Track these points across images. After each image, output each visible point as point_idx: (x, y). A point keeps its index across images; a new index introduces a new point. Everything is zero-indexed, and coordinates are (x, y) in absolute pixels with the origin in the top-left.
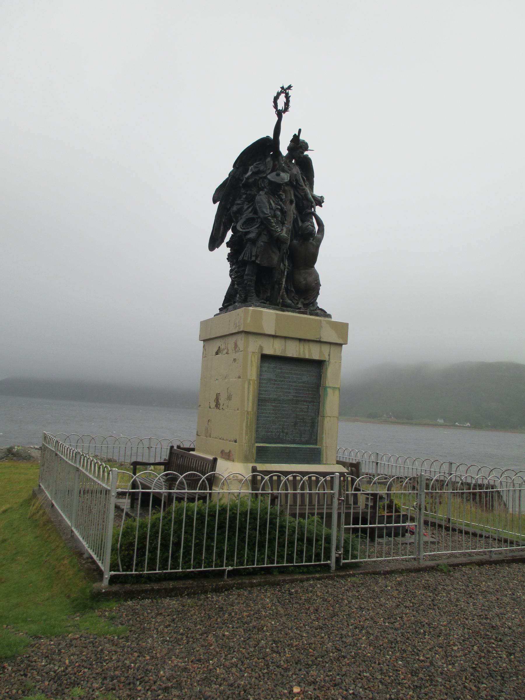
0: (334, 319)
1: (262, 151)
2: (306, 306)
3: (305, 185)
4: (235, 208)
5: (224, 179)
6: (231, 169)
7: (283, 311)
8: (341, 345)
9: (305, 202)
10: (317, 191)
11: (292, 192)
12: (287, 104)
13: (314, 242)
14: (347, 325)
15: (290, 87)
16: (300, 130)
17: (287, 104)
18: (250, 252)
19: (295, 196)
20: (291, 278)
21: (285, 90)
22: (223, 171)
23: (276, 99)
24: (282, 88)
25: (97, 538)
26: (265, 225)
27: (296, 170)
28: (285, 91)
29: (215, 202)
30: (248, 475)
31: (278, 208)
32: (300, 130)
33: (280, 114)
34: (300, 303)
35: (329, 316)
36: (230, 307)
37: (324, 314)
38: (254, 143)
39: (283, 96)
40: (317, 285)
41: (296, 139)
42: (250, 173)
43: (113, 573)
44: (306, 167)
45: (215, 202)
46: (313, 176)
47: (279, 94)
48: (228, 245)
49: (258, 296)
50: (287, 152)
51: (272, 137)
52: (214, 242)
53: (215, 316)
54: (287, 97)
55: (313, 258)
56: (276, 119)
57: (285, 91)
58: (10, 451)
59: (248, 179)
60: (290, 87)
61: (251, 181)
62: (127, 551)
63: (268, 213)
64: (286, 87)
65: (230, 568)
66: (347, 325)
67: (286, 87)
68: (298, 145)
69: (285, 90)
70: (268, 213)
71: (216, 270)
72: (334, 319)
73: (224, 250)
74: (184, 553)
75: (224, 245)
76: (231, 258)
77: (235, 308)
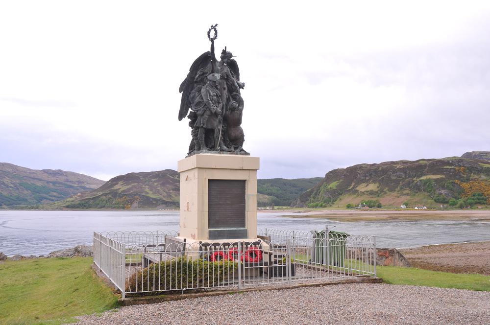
0: (251, 156)
1: (206, 60)
2: (236, 148)
3: (234, 77)
4: (191, 96)
5: (185, 79)
6: (188, 72)
7: (220, 154)
8: (256, 170)
9: (233, 87)
10: (241, 81)
11: (225, 83)
12: (216, 34)
13: (238, 112)
14: (259, 158)
15: (216, 25)
16: (226, 47)
17: (216, 34)
18: (201, 121)
19: (227, 84)
20: (225, 133)
21: (214, 27)
22: (184, 73)
23: (209, 33)
24: (212, 26)
25: (120, 279)
26: (206, 106)
27: (227, 69)
28: (214, 28)
29: (180, 92)
30: (198, 246)
31: (214, 95)
32: (226, 47)
33: (212, 40)
34: (232, 148)
35: (248, 154)
36: (192, 153)
37: (246, 153)
38: (198, 58)
39: (213, 30)
40: (243, 136)
41: (224, 52)
42: (198, 76)
43: (127, 292)
44: (233, 66)
45: (180, 92)
46: (238, 70)
47: (210, 30)
48: (188, 117)
49: (207, 146)
50: (221, 59)
51: (210, 51)
52: (181, 116)
53: (186, 157)
54: (216, 31)
55: (238, 121)
56: (210, 43)
57: (214, 28)
58: (77, 250)
59: (197, 79)
60: (216, 25)
61: (199, 79)
62: (133, 284)
63: (212, 97)
64: (214, 25)
65: (185, 289)
66: (259, 158)
67: (214, 25)
68: (226, 55)
69: (214, 27)
70: (212, 97)
71: (184, 132)
72: (251, 156)
73: (187, 120)
74: (155, 281)
75: (186, 117)
76: (191, 124)
77: (194, 154)
